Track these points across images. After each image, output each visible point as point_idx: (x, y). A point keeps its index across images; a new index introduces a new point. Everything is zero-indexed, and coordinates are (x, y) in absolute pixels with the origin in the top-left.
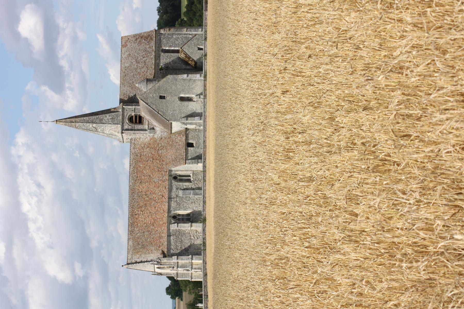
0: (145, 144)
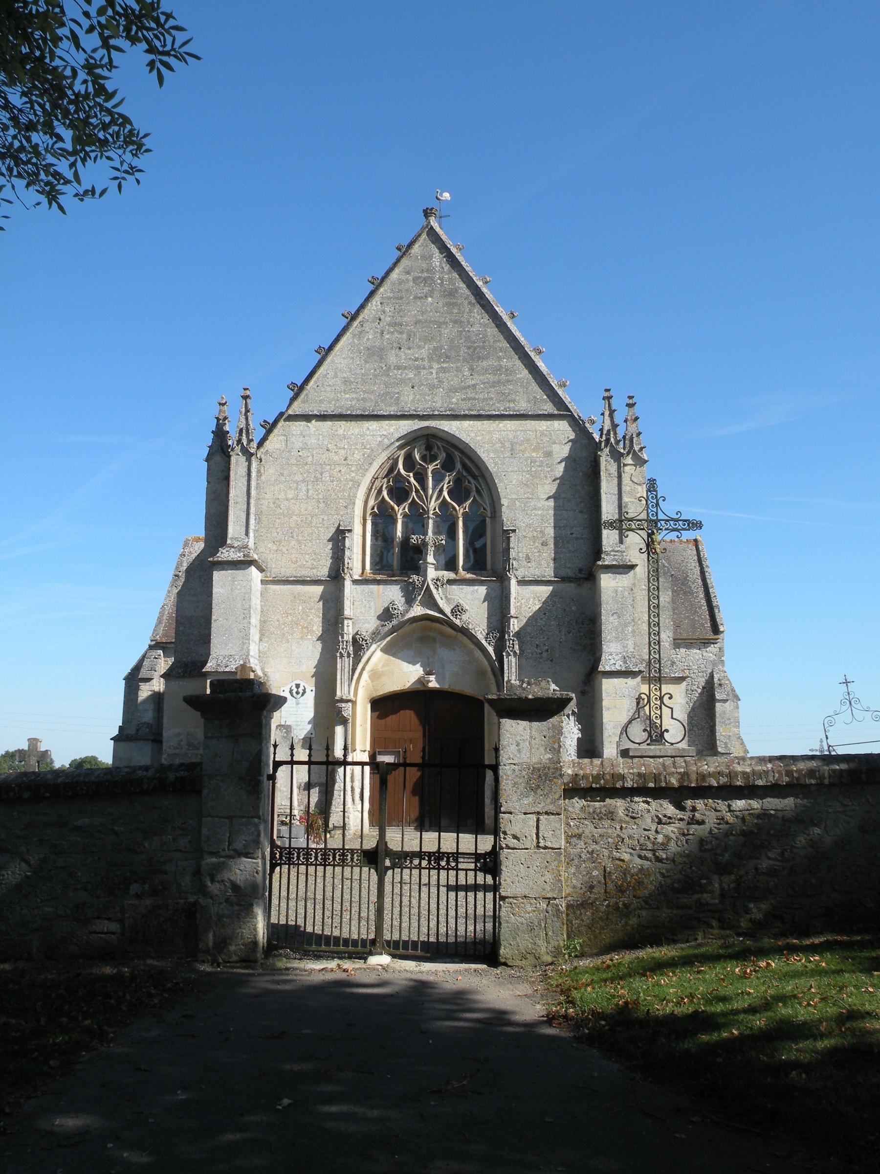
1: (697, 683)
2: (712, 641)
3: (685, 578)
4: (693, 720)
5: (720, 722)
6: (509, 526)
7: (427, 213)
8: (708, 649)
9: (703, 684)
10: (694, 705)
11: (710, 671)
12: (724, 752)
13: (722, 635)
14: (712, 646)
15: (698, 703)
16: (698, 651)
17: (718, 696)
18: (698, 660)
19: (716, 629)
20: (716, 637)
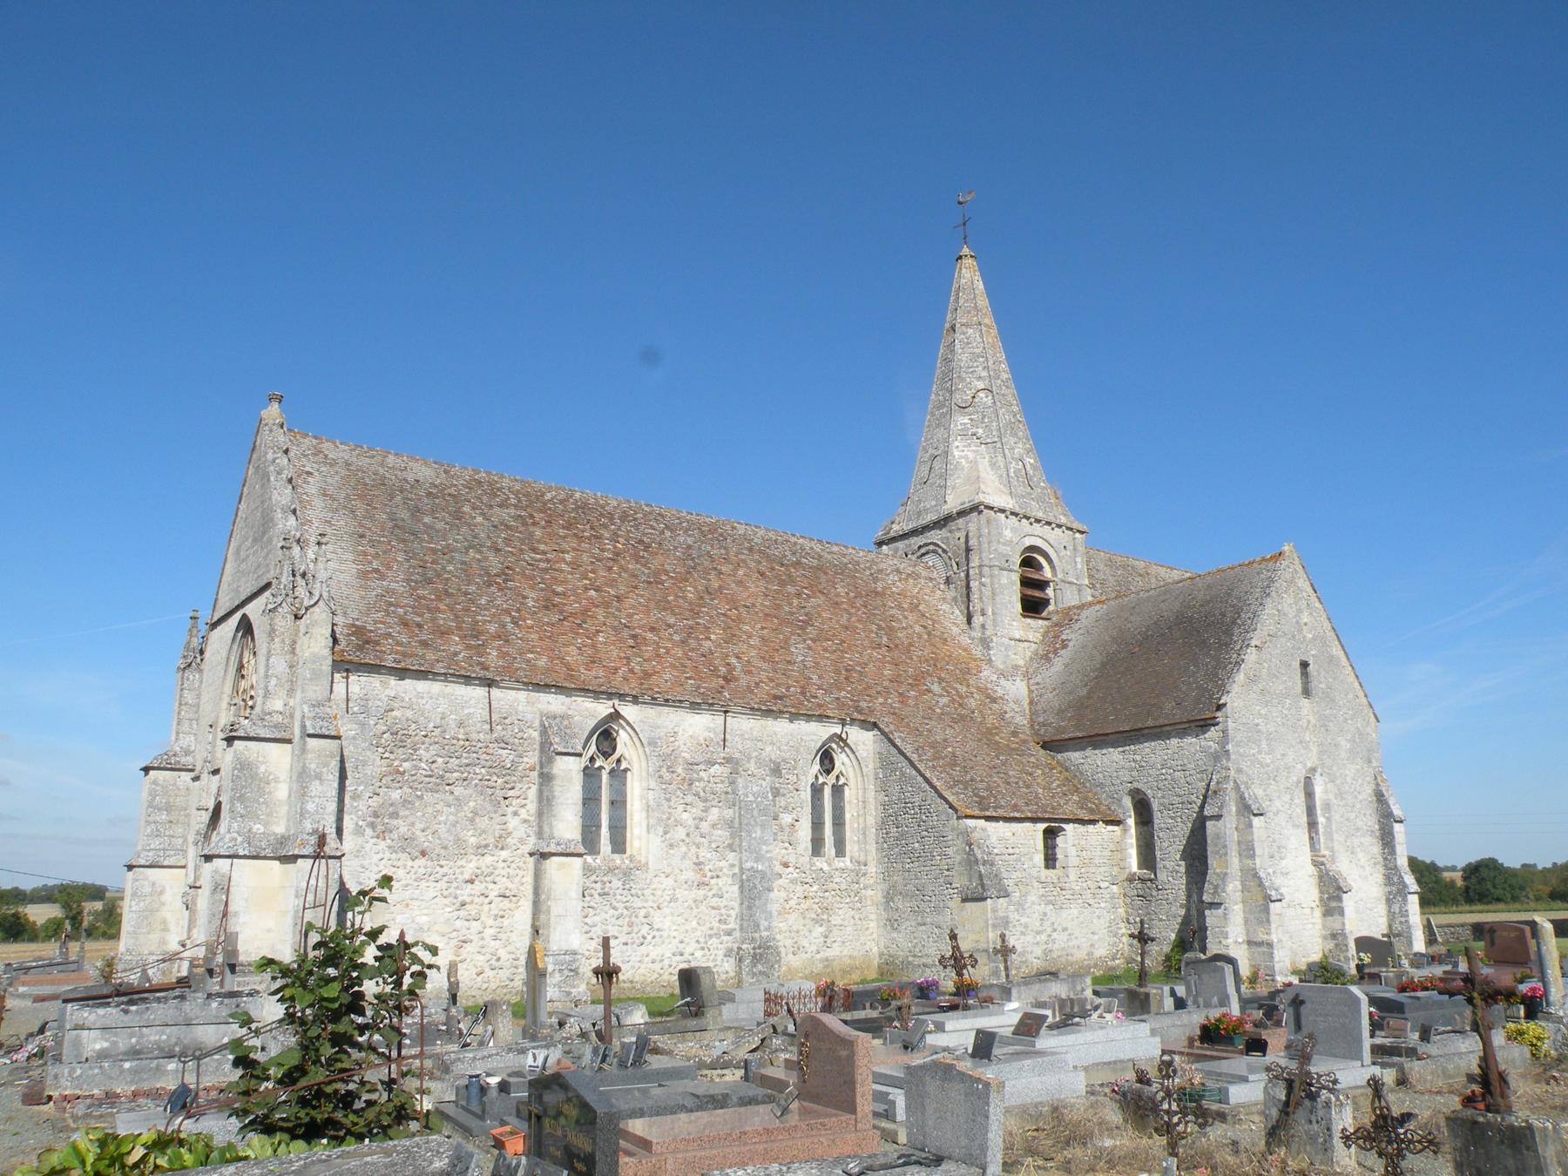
0: (934, 622)
2: (1209, 722)
5: (1212, 852)
6: (1058, 814)
8: (1206, 736)
10: (1193, 825)
14: (1213, 728)
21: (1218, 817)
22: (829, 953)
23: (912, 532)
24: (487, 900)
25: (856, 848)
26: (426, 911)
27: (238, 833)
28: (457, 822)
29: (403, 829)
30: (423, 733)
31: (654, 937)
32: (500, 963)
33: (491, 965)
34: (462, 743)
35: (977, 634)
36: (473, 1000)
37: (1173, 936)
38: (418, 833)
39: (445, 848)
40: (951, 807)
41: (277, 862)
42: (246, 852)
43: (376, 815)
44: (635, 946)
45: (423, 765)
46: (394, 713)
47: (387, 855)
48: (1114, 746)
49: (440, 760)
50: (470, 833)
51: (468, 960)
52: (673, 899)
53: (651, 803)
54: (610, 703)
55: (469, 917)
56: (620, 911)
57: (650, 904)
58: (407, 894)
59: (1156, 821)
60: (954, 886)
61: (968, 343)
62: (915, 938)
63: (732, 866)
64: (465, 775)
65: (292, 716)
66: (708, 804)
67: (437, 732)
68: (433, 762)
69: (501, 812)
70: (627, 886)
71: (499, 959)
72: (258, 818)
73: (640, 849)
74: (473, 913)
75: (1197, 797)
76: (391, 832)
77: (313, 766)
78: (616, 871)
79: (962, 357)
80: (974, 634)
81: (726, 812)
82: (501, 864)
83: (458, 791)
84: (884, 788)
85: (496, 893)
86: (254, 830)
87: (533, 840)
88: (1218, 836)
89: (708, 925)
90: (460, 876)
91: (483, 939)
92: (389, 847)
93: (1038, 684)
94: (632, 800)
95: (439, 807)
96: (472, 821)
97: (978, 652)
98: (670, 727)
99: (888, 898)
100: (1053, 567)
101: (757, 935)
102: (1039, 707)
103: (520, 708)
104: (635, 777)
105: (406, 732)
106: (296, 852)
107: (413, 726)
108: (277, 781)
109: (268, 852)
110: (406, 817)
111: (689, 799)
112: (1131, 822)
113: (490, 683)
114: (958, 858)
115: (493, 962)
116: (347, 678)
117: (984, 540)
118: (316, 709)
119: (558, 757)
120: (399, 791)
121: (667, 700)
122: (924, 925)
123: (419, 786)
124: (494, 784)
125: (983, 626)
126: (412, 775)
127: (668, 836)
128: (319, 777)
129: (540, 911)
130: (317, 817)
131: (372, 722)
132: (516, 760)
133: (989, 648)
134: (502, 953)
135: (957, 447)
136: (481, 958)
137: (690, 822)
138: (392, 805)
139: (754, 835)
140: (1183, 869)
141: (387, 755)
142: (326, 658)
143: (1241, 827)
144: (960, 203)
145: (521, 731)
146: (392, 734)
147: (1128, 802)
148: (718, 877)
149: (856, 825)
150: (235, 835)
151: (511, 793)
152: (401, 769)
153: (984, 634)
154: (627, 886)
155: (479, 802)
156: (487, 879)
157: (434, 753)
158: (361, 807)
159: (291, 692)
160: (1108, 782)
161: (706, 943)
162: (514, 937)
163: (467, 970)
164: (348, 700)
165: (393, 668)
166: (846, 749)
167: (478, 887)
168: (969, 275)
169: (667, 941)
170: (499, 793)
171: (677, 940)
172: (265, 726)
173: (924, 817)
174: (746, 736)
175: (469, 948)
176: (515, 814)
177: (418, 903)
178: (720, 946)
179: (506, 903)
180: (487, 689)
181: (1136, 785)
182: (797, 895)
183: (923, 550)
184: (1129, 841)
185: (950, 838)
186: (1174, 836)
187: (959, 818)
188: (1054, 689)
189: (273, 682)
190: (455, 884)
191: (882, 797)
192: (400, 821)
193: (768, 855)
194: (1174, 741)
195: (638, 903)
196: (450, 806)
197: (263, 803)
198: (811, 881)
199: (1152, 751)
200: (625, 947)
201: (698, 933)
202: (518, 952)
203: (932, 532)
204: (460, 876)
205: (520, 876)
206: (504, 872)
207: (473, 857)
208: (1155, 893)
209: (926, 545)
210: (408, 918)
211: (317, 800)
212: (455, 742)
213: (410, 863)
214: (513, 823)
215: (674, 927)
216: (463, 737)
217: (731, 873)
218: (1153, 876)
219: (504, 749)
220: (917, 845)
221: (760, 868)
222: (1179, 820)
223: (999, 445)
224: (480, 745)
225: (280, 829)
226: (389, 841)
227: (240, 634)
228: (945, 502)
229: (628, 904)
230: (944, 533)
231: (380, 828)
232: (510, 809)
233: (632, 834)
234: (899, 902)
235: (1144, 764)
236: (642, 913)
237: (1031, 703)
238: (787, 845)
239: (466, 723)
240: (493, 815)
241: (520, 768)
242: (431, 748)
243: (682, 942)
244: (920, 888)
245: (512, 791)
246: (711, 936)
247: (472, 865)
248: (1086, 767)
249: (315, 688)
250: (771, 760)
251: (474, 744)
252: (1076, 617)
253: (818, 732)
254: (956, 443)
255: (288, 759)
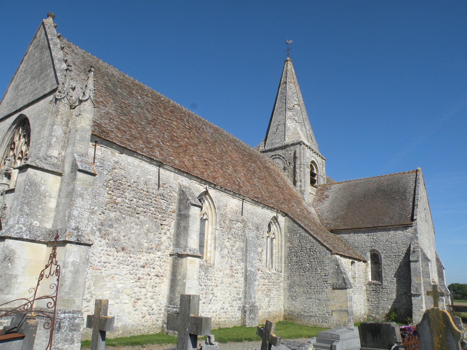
1: (402, 251)
2: (409, 225)
3: (405, 192)
4: (400, 273)
5: (414, 275)
7: (91, 67)
8: (407, 231)
9: (405, 252)
11: (409, 243)
12: (415, 293)
13: (415, 221)
14: (410, 228)
15: (402, 263)
16: (401, 232)
17: (411, 259)
18: (401, 237)
19: (412, 219)
20: (411, 223)
21: (417, 261)
22: (270, 309)
23: (269, 150)
24: (150, 277)
25: (277, 264)
26: (121, 281)
27: (24, 225)
28: (140, 234)
29: (114, 235)
30: (128, 184)
31: (214, 300)
32: (153, 311)
33: (149, 312)
34: (145, 193)
35: (298, 188)
36: (140, 332)
37: (390, 307)
38: (122, 237)
39: (133, 247)
40: (328, 249)
41: (45, 246)
42: (28, 237)
43: (102, 225)
44: (207, 304)
45: (127, 201)
46: (116, 171)
47: (105, 248)
48: (364, 232)
49: (135, 200)
50: (145, 241)
51: (139, 310)
52: (222, 283)
53: (217, 236)
54: (205, 186)
55: (141, 286)
56: (203, 287)
57: (213, 284)
58: (113, 271)
59: (383, 262)
60: (328, 282)
61: (291, 88)
62: (305, 304)
63: (242, 268)
64: (146, 210)
65: (63, 161)
66: (236, 240)
67: (135, 185)
68: (131, 201)
69: (159, 232)
70: (206, 275)
71: (153, 309)
72: (37, 218)
73: (210, 257)
74: (143, 284)
75: (402, 254)
76: (108, 235)
77: (79, 189)
78: (203, 267)
79: (289, 93)
80: (297, 188)
81: (241, 244)
82: (157, 259)
83: (142, 218)
84: (289, 240)
85: (154, 274)
86: (34, 224)
87: (172, 248)
88: (416, 269)
89: (233, 295)
90: (138, 263)
91: (146, 298)
92: (107, 244)
93: (319, 209)
94: (208, 234)
95: (132, 225)
96: (147, 234)
97: (299, 194)
98: (225, 202)
99: (291, 287)
100: (317, 170)
101: (250, 301)
102: (323, 218)
103: (171, 181)
104: (210, 224)
105: (120, 182)
106: (67, 239)
107: (124, 180)
108: (50, 196)
109: (41, 239)
110: (117, 228)
111: (230, 236)
112: (369, 262)
113: (160, 164)
114: (331, 271)
115: (150, 311)
116: (95, 146)
117: (302, 155)
118: (82, 158)
119: (192, 207)
120: (114, 213)
121: (225, 189)
122: (311, 299)
123: (124, 212)
124: (157, 217)
125: (301, 186)
126: (122, 206)
127: (222, 252)
128: (82, 196)
129: (177, 285)
130: (78, 220)
131: (105, 173)
132: (168, 206)
133: (303, 194)
134: (154, 306)
135: (289, 122)
136: (144, 308)
137: (229, 247)
138: (110, 220)
139: (251, 255)
140: (395, 281)
141: (110, 192)
142: (88, 131)
143: (424, 266)
144: (287, 43)
145: (170, 192)
146: (114, 181)
147: (369, 254)
148: (238, 273)
149: (277, 255)
150: (22, 226)
151: (164, 223)
152: (117, 201)
153: (301, 189)
154: (206, 275)
155: (150, 225)
156: (151, 266)
157: (132, 195)
158: (95, 219)
159: (64, 147)
160: (360, 247)
161: (232, 303)
162: (160, 298)
163: (138, 315)
164: (94, 158)
165: (120, 146)
166: (276, 223)
167: (147, 270)
168: (290, 66)
169: (219, 302)
170: (159, 222)
171: (222, 302)
172: (47, 163)
173: (312, 253)
174: (249, 212)
175: (140, 303)
176: (165, 233)
177: (118, 276)
178: (236, 305)
179: (158, 280)
180: (158, 168)
181: (373, 248)
182: (261, 284)
183: (273, 157)
184: (369, 269)
185: (327, 262)
186: (391, 268)
187: (332, 254)
188: (328, 212)
189: (54, 139)
190: (136, 268)
191: (289, 244)
192: (113, 230)
193: (255, 265)
194: (392, 232)
195: (209, 283)
196: (137, 225)
197: (41, 208)
198: (266, 277)
199: (382, 236)
200: (204, 305)
201: (229, 299)
202: (161, 306)
203: (278, 151)
204: (138, 263)
205: (165, 266)
206: (158, 263)
207: (145, 254)
208: (381, 290)
209: (274, 155)
210: (113, 285)
211: (79, 209)
212: (142, 191)
213: (116, 254)
214: (164, 238)
215: (222, 296)
216: (146, 190)
217: (242, 272)
218: (380, 283)
219: (163, 200)
220: (308, 265)
221: (253, 270)
222: (394, 262)
223: (303, 124)
224: (153, 195)
225: (49, 225)
226: (107, 240)
227: (14, 127)
228: (285, 140)
229: (206, 284)
230: (284, 151)
231: (103, 232)
232: (163, 231)
233: (207, 250)
234: (296, 288)
235: (378, 240)
236: (211, 288)
237: (319, 216)
238: (259, 261)
239: (148, 183)
240: (156, 233)
241: (169, 211)
242: (131, 193)
243: (224, 303)
244: (309, 283)
245: (164, 222)
246: (234, 300)
247: (144, 258)
248: (350, 240)
249: (81, 146)
250: (256, 223)
251: (151, 194)
252: (329, 188)
253: (271, 214)
254: (288, 121)
255: (58, 185)
